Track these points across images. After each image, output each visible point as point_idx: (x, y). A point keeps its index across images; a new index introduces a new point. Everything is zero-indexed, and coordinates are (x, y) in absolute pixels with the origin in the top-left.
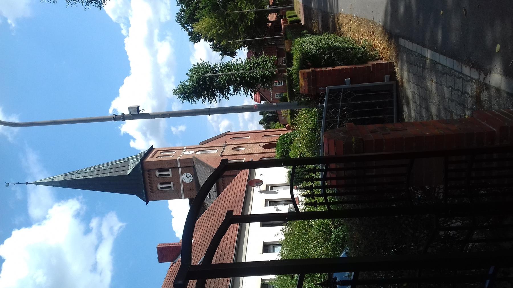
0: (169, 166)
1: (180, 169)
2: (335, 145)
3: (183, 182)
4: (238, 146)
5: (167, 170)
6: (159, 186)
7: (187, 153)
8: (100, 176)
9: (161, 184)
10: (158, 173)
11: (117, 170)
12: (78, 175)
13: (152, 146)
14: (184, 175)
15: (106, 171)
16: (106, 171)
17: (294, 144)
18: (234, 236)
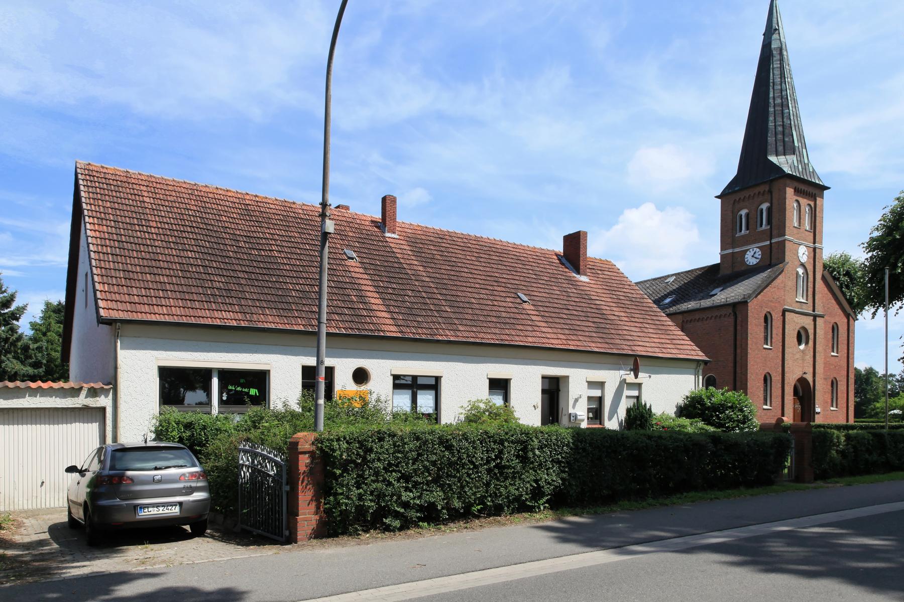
4: (811, 337)
5: (769, 222)
6: (743, 212)
8: (771, 109)
9: (747, 215)
10: (765, 206)
11: (780, 137)
12: (777, 72)
13: (828, 188)
15: (779, 119)
16: (779, 119)
18: (530, 339)
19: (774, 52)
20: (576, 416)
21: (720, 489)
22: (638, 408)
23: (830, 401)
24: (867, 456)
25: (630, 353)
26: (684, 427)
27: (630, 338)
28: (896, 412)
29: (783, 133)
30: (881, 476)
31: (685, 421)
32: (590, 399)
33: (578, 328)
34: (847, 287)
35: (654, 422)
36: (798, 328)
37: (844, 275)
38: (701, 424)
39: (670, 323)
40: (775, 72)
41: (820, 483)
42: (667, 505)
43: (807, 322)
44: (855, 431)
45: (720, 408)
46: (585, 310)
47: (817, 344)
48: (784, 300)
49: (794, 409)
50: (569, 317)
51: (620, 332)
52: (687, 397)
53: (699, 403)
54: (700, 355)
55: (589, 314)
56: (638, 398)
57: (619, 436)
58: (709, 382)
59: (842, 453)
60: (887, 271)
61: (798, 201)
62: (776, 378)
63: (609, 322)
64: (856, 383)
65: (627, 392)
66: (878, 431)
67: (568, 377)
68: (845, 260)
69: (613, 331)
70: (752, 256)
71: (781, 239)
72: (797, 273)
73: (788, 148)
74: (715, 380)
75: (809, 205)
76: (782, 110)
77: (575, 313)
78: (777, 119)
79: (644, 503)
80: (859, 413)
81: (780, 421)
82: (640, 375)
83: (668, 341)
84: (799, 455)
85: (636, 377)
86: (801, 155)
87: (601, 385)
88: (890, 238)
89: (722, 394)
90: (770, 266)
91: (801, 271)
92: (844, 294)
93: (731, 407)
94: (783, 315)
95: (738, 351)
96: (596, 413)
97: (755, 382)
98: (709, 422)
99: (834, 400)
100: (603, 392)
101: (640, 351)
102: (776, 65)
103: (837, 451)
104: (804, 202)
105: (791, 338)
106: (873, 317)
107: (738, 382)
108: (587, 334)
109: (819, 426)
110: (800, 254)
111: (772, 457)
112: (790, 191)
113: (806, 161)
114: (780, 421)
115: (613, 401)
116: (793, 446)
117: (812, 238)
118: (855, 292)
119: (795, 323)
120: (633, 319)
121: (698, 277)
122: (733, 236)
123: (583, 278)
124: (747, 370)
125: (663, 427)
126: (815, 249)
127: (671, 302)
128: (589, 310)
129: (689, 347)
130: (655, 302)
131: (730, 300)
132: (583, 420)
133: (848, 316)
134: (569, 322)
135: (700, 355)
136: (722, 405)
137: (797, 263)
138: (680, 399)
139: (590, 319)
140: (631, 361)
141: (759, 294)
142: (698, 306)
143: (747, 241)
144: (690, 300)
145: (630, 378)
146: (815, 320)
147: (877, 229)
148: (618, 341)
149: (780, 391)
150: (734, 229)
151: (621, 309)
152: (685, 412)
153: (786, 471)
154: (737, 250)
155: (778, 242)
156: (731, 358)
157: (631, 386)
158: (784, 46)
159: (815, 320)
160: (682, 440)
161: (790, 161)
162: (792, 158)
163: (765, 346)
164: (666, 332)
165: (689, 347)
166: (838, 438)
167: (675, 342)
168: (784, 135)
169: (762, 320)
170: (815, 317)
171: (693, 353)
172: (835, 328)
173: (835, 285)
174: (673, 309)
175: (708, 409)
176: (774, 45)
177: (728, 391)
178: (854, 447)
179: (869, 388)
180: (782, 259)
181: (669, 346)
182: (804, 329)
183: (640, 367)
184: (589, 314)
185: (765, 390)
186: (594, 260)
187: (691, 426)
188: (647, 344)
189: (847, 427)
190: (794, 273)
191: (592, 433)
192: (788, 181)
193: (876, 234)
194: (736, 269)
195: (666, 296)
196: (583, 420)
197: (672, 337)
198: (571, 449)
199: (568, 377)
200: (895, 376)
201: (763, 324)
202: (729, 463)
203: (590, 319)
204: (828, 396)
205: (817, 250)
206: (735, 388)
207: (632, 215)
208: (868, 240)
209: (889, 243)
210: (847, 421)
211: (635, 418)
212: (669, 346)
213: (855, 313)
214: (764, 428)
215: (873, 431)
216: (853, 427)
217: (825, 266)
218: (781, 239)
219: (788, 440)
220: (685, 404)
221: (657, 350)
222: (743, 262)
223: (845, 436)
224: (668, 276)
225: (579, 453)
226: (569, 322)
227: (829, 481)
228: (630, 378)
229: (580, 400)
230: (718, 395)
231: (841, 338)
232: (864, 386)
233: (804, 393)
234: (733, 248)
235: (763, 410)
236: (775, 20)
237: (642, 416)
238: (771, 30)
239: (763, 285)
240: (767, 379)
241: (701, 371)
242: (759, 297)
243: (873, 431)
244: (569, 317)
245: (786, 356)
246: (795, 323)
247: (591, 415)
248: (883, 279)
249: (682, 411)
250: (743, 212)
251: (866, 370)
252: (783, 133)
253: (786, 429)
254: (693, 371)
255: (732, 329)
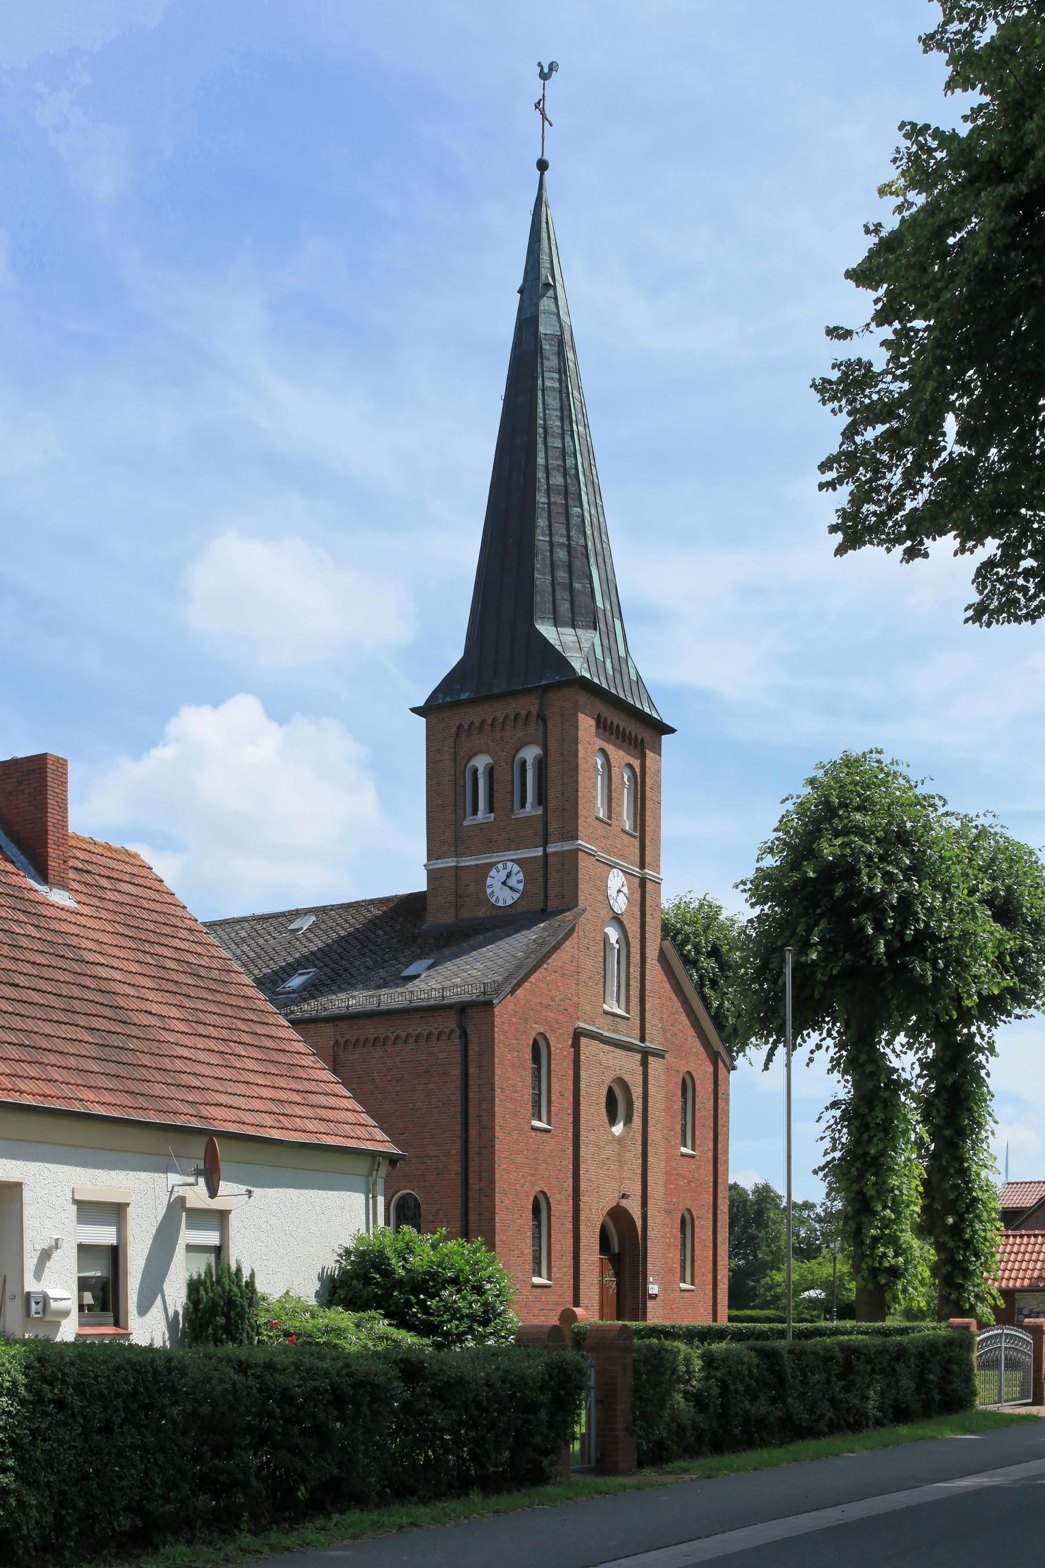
0: (552, 804)
1: (539, 852)
2: (709, 1477)
3: (493, 865)
4: (638, 1104)
5: (541, 799)
6: (481, 762)
7: (616, 881)
8: (541, 499)
9: (491, 771)
10: (530, 754)
11: (562, 575)
12: (553, 402)
13: (672, 731)
14: (516, 868)
15: (560, 528)
16: (560, 528)
17: (204, 1548)
19: (546, 347)
20: (45, 1299)
21: (424, 1501)
22: (219, 1281)
23: (677, 1266)
24: (747, 1404)
25: (195, 1123)
26: (340, 1332)
27: (194, 1082)
28: (812, 1293)
29: (570, 568)
30: (775, 1452)
31: (342, 1317)
32: (84, 1250)
33: (44, 1043)
34: (714, 984)
35: (262, 1321)
36: (608, 1080)
37: (710, 955)
38: (382, 1326)
39: (301, 1047)
40: (549, 400)
41: (649, 1474)
42: (288, 1549)
43: (628, 1065)
44: (723, 1345)
45: (426, 1284)
46: (65, 990)
47: (651, 1123)
48: (577, 1006)
49: (602, 1286)
50: (19, 1008)
51: (167, 1063)
52: (348, 1252)
53: (377, 1268)
54: (379, 1141)
55: (78, 1006)
56: (219, 1251)
57: (160, 1364)
58: (405, 1212)
59: (698, 1400)
60: (789, 957)
61: (603, 751)
62: (561, 1206)
63: (134, 1031)
64: (732, 1225)
65: (188, 1236)
66: (768, 1344)
67: (17, 1187)
68: (709, 914)
69: (145, 1060)
70: (504, 885)
71: (567, 846)
72: (606, 939)
73: (583, 613)
74: (417, 1206)
75: (630, 766)
76: (567, 507)
77: (36, 997)
78: (555, 526)
79: (230, 1548)
80: (739, 1296)
81: (567, 1316)
82: (225, 1187)
83: (296, 1097)
84: (606, 1404)
85: (213, 1192)
86: (609, 635)
87: (115, 1212)
88: (796, 876)
89: (434, 1247)
90: (544, 913)
91: (613, 934)
92: (705, 999)
93: (454, 1281)
94: (576, 1045)
95: (473, 1132)
96: (104, 1295)
97: (511, 1216)
98: (402, 1321)
99: (687, 1264)
100: (121, 1234)
101: (223, 1120)
102: (551, 381)
103: (686, 1393)
104: (619, 756)
105: (594, 1107)
106: (766, 1067)
107: (473, 1220)
108: (72, 1062)
109: (654, 1332)
110: (612, 892)
111: (543, 1413)
112: (586, 724)
113: (622, 653)
114: (567, 1316)
115: (149, 1259)
116: (592, 1383)
117: (637, 851)
118: (731, 1000)
119: (603, 1066)
120: (201, 1030)
121: (374, 924)
122: (457, 823)
123: (59, 897)
124: (493, 1182)
125: (287, 1334)
126: (643, 882)
127: (304, 987)
128: (77, 992)
129: (350, 1117)
130: (261, 983)
131: (454, 996)
132: (66, 1314)
133: (714, 1057)
134: (18, 1023)
135: (379, 1141)
136: (434, 1275)
137: (604, 913)
138: (327, 1259)
139: (82, 1021)
140: (199, 1147)
141: (519, 984)
142: (371, 1005)
143: (493, 840)
144: (353, 986)
145: (197, 1195)
146: (644, 1064)
147: (771, 850)
148: (160, 1090)
149: (570, 1242)
150: (457, 805)
151: (169, 998)
152: (342, 1293)
153: (577, 1446)
154: (467, 862)
155: (563, 853)
156: (456, 1149)
157: (200, 1217)
158: (567, 336)
159: (644, 1064)
160: (326, 1374)
161: (586, 645)
162: (590, 638)
163: (536, 1123)
164: (291, 1070)
165: (350, 1117)
166: (688, 1361)
167: (314, 1099)
168: (570, 573)
169: (528, 1056)
170: (646, 1055)
171: (360, 1132)
172: (687, 1086)
173: (689, 979)
174: (308, 1008)
175: (399, 1284)
176: (546, 327)
177: (446, 1238)
178: (724, 1387)
179: (762, 1234)
180: (570, 902)
181: (299, 1111)
182: (620, 1081)
183: (223, 1167)
184: (78, 1006)
185: (537, 1238)
186: (88, 846)
187: (362, 1333)
188: (242, 1103)
189: (705, 1335)
190: (599, 937)
191: (81, 1357)
192: (583, 698)
193: (770, 862)
194: (465, 914)
195: (290, 970)
196: (66, 1314)
197: (308, 1086)
198: (22, 1402)
199: (17, 1187)
200: (812, 1206)
201: (530, 1064)
202: (443, 1431)
203: (82, 1021)
204: (675, 1254)
205: (649, 884)
206: (466, 1234)
207: (196, 722)
208: (750, 874)
209: (795, 889)
210: (715, 1319)
211: (213, 1309)
212: (299, 1111)
213: (729, 1051)
214: (526, 1339)
215: (760, 1344)
216: (720, 1335)
217: (667, 929)
218: (567, 846)
219: (580, 1371)
220: (344, 1272)
221: (268, 1120)
222: (482, 898)
223: (702, 1357)
224: (297, 914)
225: (45, 1413)
226: (18, 1023)
227: (667, 1467)
228: (197, 1195)
229: (56, 1255)
230: (425, 1250)
231: (704, 1116)
232: (752, 1230)
233: (623, 1246)
234: (457, 855)
235: (533, 1291)
236: (545, 263)
237: (231, 1303)
238: (537, 286)
239: (531, 963)
240: (539, 1208)
241: (380, 1184)
242: (519, 992)
243: (760, 1344)
244: (19, 1008)
245: (583, 1149)
246: (603, 1066)
247: (88, 1298)
248: (780, 974)
249: (338, 1290)
250: (481, 762)
251: (757, 1191)
252: (570, 568)
253: (580, 1339)
254: (361, 1181)
255: (456, 1072)
